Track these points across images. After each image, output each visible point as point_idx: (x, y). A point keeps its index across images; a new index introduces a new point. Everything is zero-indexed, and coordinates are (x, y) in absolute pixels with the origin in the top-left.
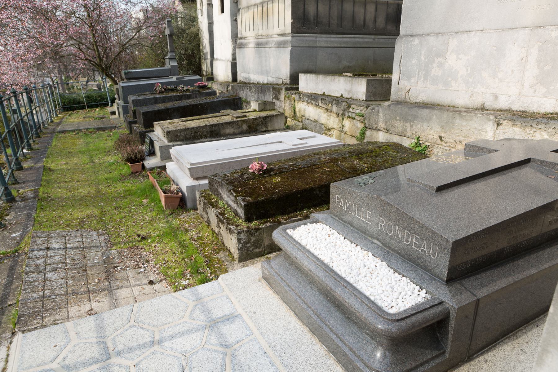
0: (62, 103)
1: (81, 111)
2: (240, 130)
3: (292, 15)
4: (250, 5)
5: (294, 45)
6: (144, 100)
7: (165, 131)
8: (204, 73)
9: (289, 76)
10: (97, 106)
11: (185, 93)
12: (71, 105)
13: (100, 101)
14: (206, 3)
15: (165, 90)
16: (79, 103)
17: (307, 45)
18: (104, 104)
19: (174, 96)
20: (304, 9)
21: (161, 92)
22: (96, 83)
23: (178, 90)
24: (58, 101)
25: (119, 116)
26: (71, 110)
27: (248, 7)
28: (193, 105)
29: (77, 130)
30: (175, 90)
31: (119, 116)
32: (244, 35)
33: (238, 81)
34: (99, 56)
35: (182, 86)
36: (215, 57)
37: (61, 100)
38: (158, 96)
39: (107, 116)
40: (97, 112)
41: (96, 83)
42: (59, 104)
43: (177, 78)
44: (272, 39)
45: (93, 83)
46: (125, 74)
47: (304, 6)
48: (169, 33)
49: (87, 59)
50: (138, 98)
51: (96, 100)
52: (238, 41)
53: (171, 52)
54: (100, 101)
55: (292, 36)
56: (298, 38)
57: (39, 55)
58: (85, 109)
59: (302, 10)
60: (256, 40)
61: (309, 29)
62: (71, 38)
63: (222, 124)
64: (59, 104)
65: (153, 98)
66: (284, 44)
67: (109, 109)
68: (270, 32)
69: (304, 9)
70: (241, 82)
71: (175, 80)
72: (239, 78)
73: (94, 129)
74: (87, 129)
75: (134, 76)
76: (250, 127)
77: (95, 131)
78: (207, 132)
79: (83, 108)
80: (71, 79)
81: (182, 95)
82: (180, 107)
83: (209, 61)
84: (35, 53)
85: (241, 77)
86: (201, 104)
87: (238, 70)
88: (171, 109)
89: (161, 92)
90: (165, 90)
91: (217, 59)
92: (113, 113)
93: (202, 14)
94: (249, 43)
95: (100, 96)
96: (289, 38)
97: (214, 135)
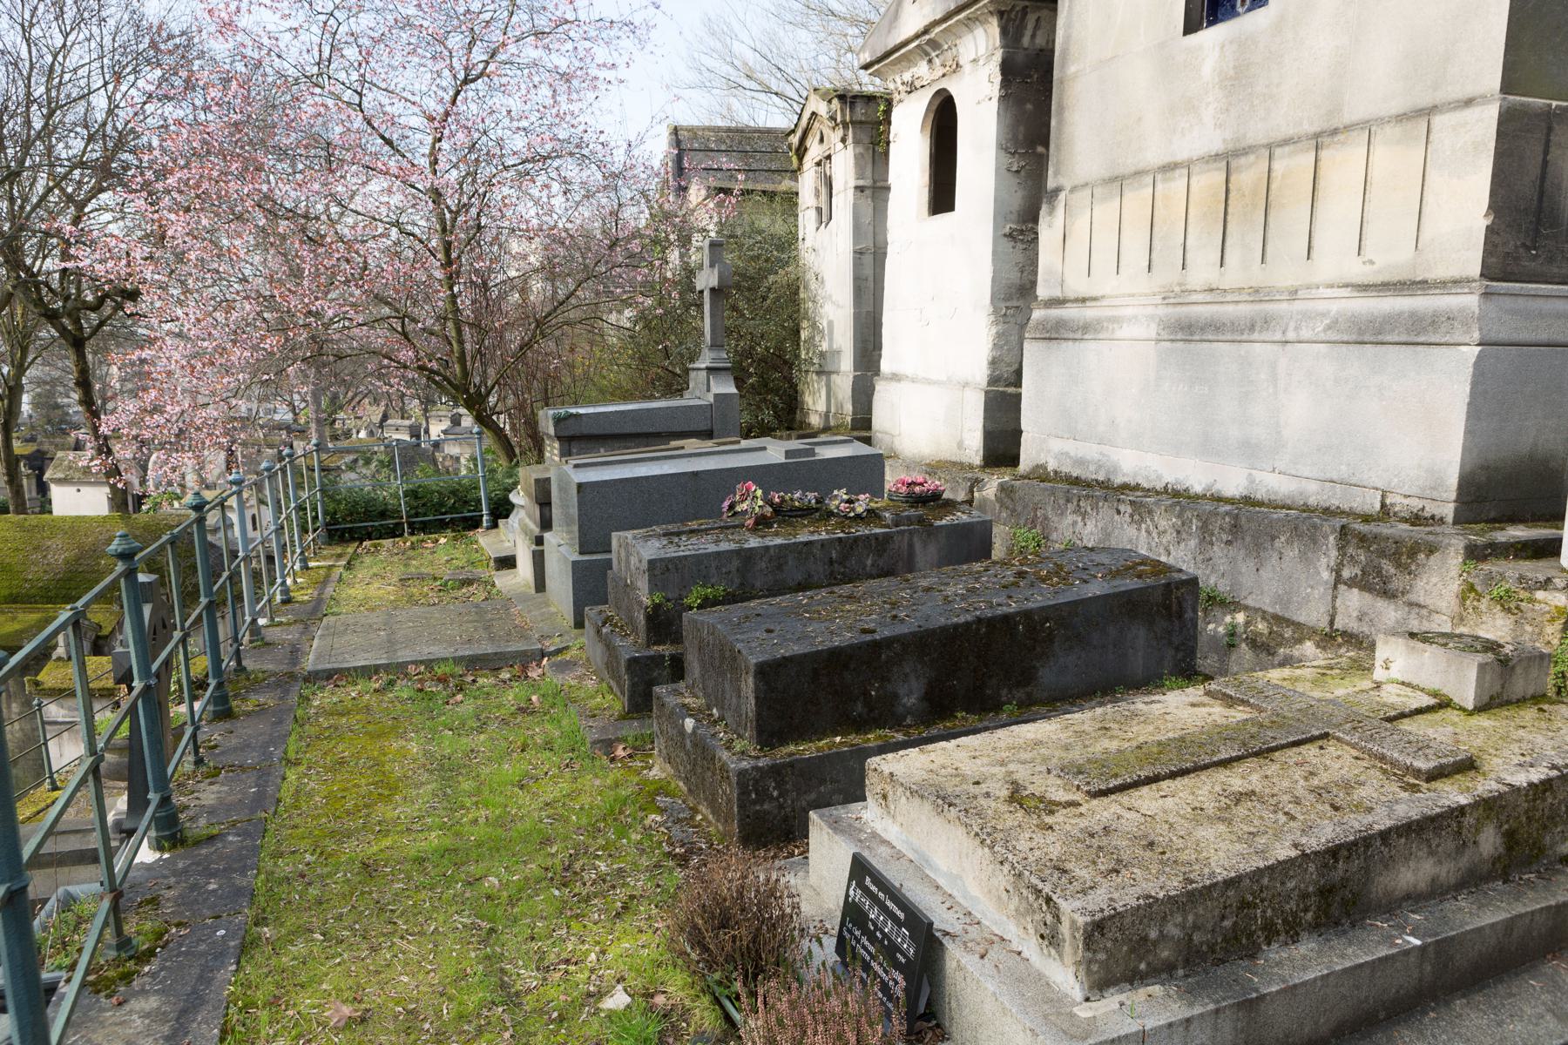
0: (325, 513)
1: (387, 543)
2: (1464, 862)
3: (1493, 193)
4: (1128, 164)
5: (1493, 336)
6: (699, 560)
7: (1074, 912)
8: (815, 420)
9: (1453, 481)
10: (441, 526)
11: (862, 531)
12: (352, 525)
13: (453, 509)
14: (852, 183)
15: (778, 510)
16: (383, 514)
17: (1543, 336)
18: (465, 519)
19: (823, 543)
20: (1545, 163)
21: (762, 523)
22: (407, 423)
23: (831, 514)
24: (315, 509)
25: (540, 584)
26: (353, 539)
27: (1118, 182)
28: (992, 623)
29: (387, 668)
30: (817, 513)
31: (540, 584)
32: (1077, 285)
33: (1025, 464)
34: (462, 359)
35: (842, 494)
36: (886, 366)
37: (323, 503)
38: (754, 542)
39: (484, 572)
40: (442, 553)
41: (407, 423)
42: (315, 518)
43: (788, 454)
44: (1298, 306)
45: (399, 422)
46: (558, 421)
47: (1546, 152)
48: (714, 282)
49: (422, 368)
50: (672, 552)
51: (442, 504)
52: (1037, 314)
53: (715, 346)
54: (453, 509)
55: (1487, 295)
56: (1508, 302)
57: (272, 354)
58: (401, 535)
59: (1534, 170)
60: (1162, 311)
61: (1551, 260)
62: (380, 300)
63: (1384, 836)
64: (315, 518)
65: (738, 552)
66: (1424, 330)
67: (489, 542)
68: (1284, 273)
69: (1545, 163)
70: (1040, 474)
71: (781, 459)
72: (1029, 455)
73: (457, 660)
74: (429, 664)
75: (586, 431)
76: (1511, 838)
77: (459, 670)
78: (1304, 896)
79: (395, 532)
80: (341, 408)
81: (856, 539)
82: (931, 633)
83: (844, 383)
84: (255, 348)
85: (1040, 445)
86: (1027, 615)
87: (1025, 424)
88: (888, 642)
89: (762, 523)
90: (778, 510)
91: (896, 377)
92: (507, 563)
93: (824, 216)
94: (1115, 320)
95: (454, 492)
96: (1470, 301)
97: (1335, 910)
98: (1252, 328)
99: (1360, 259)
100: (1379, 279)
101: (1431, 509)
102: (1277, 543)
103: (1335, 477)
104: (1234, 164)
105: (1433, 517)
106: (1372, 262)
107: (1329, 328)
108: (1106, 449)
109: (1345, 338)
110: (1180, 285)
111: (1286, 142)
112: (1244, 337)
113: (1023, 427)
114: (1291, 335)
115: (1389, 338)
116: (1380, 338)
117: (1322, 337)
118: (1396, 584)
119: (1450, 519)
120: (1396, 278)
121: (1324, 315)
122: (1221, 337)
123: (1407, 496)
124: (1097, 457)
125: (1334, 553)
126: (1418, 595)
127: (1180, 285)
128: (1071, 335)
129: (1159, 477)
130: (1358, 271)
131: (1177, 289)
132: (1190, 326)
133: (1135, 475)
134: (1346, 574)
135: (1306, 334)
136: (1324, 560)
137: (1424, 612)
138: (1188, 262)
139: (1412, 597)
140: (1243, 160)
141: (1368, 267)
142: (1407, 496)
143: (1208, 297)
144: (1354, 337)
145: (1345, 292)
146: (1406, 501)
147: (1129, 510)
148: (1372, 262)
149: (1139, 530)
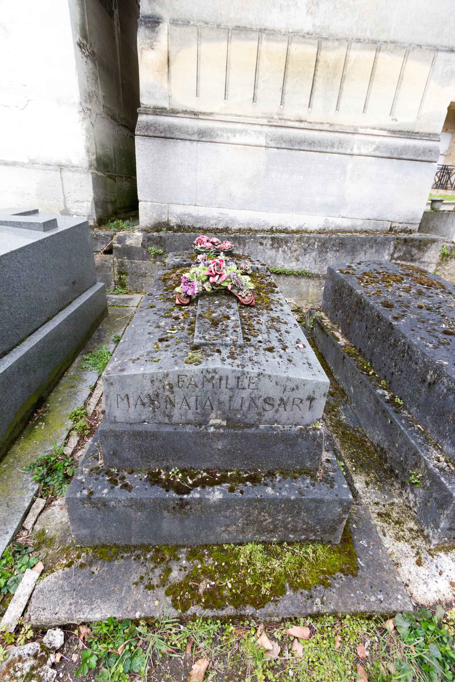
66: (420, 155)
68: (344, 119)
98: (332, 145)
99: (391, 118)
100: (398, 129)
101: (410, 227)
102: (364, 248)
103: (370, 218)
104: (324, 44)
105: (410, 230)
106: (396, 120)
107: (375, 150)
108: (224, 211)
109: (385, 155)
110: (278, 114)
111: (359, 41)
112: (329, 150)
113: (139, 198)
114: (356, 151)
115: (405, 157)
116: (401, 157)
117: (373, 153)
118: (417, 256)
119: (417, 230)
120: (406, 129)
121: (372, 143)
122: (313, 149)
123: (400, 223)
124: (216, 215)
125: (392, 248)
126: (425, 259)
127: (278, 114)
128: (188, 137)
129: (268, 224)
130: (388, 122)
131: (276, 117)
132: (290, 141)
133: (249, 224)
134: (396, 255)
135: (364, 152)
136: (387, 252)
137: (426, 264)
138: (369, 105)
139: (423, 260)
140: (330, 43)
141: (394, 123)
142: (400, 223)
143: (297, 124)
144: (388, 155)
145: (385, 133)
146: (401, 226)
147: (270, 242)
148: (396, 120)
149: (278, 251)
